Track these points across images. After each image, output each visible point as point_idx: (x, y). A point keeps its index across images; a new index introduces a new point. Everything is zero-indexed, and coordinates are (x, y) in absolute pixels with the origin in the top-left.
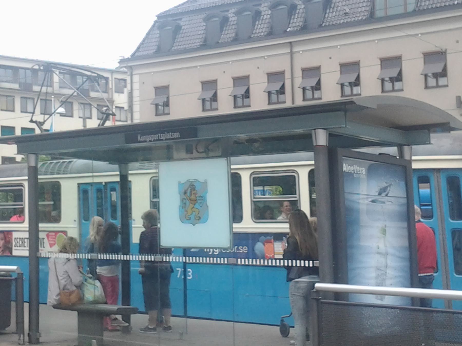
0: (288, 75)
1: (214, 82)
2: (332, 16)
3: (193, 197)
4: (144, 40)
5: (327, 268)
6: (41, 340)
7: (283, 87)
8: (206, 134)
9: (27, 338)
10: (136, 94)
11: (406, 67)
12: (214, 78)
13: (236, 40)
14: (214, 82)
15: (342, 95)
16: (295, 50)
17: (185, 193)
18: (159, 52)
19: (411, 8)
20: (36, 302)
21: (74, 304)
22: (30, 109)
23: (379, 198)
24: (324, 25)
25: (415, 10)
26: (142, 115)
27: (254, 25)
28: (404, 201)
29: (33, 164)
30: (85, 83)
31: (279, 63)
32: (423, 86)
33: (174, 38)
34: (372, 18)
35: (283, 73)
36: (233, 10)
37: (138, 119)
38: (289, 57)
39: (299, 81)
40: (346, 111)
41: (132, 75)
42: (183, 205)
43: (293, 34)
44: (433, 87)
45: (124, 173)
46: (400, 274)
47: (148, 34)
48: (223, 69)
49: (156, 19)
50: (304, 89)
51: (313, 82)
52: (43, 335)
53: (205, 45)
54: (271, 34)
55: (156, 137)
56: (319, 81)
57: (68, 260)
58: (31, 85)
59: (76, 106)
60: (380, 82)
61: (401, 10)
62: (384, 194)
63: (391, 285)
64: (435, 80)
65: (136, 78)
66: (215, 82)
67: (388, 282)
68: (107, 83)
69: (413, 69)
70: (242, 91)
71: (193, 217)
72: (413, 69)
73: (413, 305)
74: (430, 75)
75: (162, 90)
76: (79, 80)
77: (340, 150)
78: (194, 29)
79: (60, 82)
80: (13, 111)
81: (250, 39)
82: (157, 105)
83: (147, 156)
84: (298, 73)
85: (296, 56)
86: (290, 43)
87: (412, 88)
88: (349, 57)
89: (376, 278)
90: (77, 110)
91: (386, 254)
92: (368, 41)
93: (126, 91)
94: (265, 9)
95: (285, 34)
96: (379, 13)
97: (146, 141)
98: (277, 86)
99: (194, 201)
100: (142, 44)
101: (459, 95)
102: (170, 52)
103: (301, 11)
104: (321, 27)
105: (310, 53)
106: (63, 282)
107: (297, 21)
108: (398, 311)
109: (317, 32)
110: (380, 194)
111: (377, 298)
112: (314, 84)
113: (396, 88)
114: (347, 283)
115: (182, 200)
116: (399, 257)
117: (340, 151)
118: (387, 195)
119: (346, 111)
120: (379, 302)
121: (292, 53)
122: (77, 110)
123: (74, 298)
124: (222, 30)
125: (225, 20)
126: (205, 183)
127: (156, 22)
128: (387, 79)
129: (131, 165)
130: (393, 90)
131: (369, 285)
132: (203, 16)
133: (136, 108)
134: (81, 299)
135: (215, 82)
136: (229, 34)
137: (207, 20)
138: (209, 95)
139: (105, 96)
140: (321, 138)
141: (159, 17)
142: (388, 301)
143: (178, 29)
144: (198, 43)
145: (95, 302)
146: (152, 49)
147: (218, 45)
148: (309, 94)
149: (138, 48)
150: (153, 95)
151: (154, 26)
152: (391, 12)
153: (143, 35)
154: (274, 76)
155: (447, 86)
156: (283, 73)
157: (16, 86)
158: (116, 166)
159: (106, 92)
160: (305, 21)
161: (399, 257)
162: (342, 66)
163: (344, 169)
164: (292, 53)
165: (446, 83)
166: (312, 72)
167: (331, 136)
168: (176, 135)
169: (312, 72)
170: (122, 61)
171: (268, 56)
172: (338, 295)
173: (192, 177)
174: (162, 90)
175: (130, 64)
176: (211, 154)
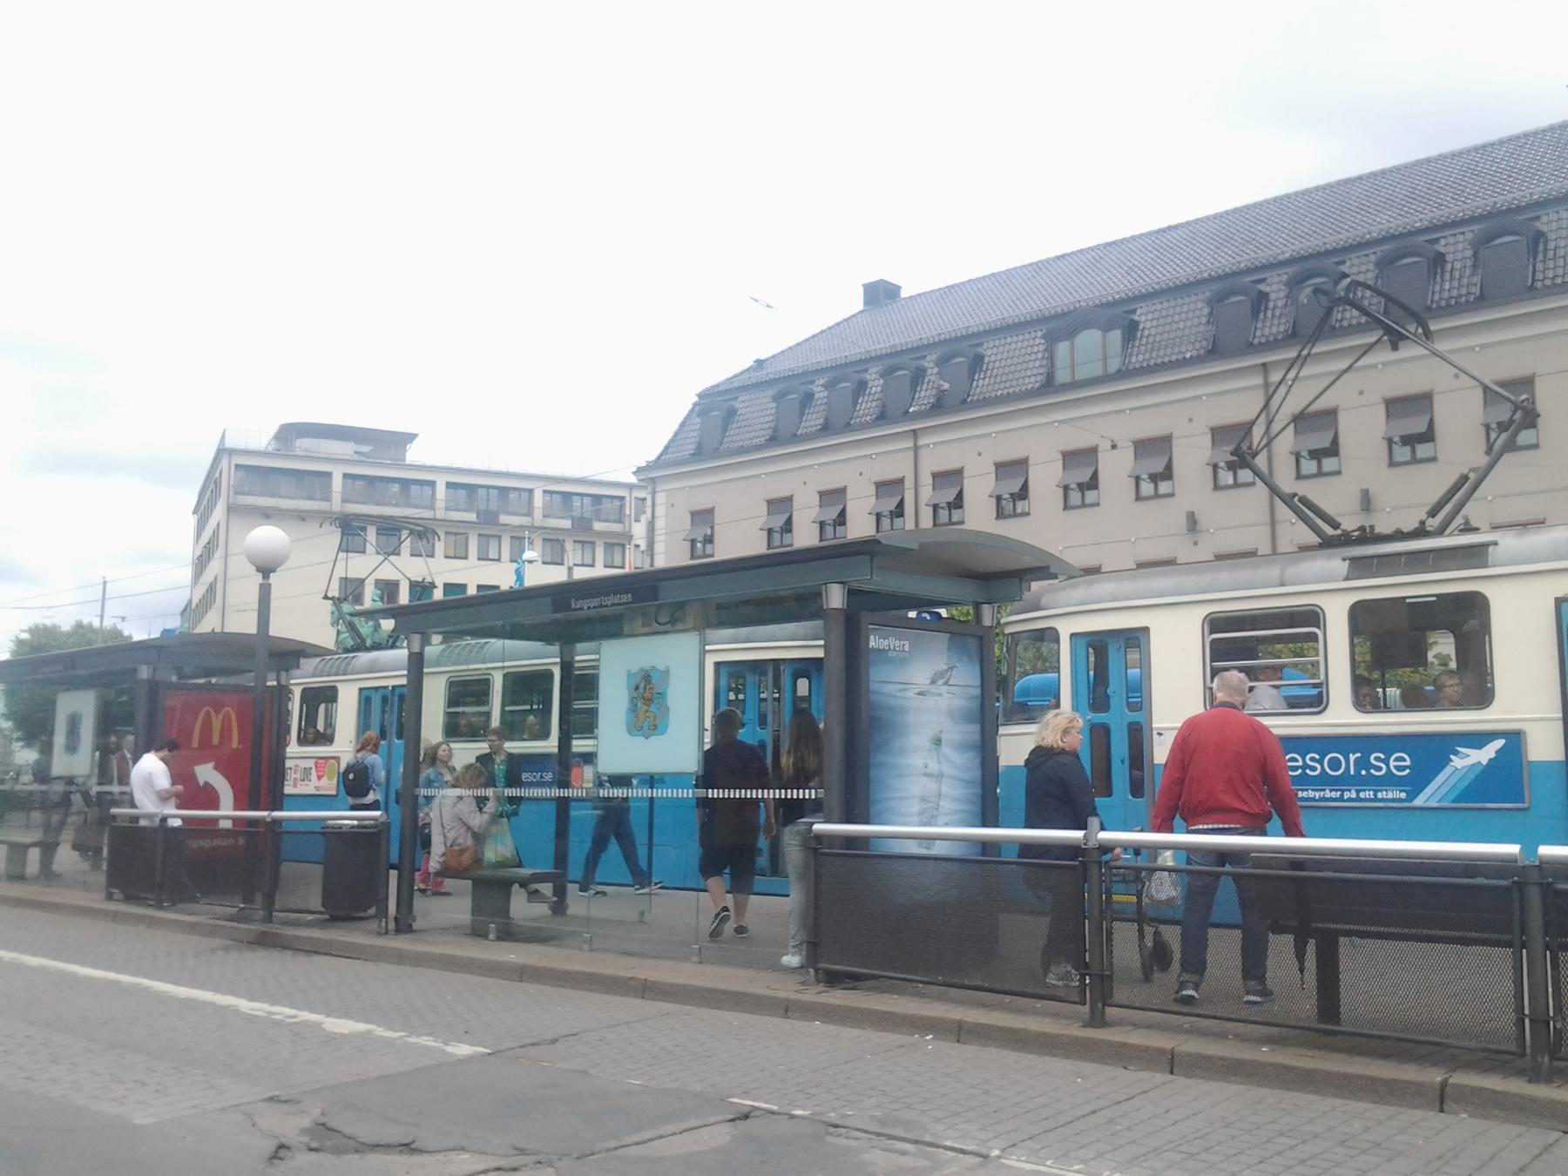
0: (909, 484)
1: (841, 492)
2: (983, 386)
3: (647, 695)
4: (676, 435)
5: (835, 803)
6: (415, 926)
7: (901, 505)
8: (670, 594)
9: (392, 925)
10: (660, 524)
11: (1443, 412)
12: (708, 506)
13: (826, 429)
14: (841, 492)
15: (769, 547)
16: (921, 443)
17: (637, 688)
18: (699, 454)
19: (1114, 365)
20: (408, 868)
21: (466, 869)
22: (493, 554)
23: (933, 688)
24: (1539, 284)
25: (1119, 371)
26: (669, 554)
27: (855, 403)
28: (978, 692)
29: (416, 649)
30: (585, 510)
31: (896, 466)
32: (1211, 485)
33: (725, 430)
34: (1049, 385)
35: (901, 481)
36: (822, 381)
37: (661, 562)
38: (911, 453)
39: (927, 493)
40: (872, 555)
41: (654, 493)
42: (633, 709)
43: (919, 416)
44: (1149, 498)
45: (567, 659)
46: (966, 807)
47: (683, 425)
48: (803, 479)
49: (696, 399)
50: (936, 507)
51: (950, 495)
52: (419, 919)
53: (774, 440)
54: (883, 417)
55: (596, 602)
56: (844, 510)
57: (460, 798)
58: (495, 515)
59: (569, 546)
60: (1133, 481)
61: (1096, 370)
62: (940, 682)
63: (946, 825)
64: (1314, 463)
65: (661, 498)
66: (790, 499)
67: (941, 820)
68: (622, 508)
69: (1046, 478)
70: (832, 513)
71: (645, 726)
72: (1046, 478)
73: (984, 854)
74: (1073, 486)
75: (702, 517)
76: (576, 503)
77: (866, 617)
78: (758, 413)
79: (544, 508)
80: (466, 558)
81: (848, 427)
82: (693, 542)
83: (610, 627)
84: (926, 479)
85: (923, 453)
86: (1264, 365)
87: (979, 516)
88: (1010, 452)
89: (921, 813)
90: (572, 554)
91: (939, 776)
92: (969, 438)
93: (643, 519)
94: (1275, 287)
95: (906, 416)
96: (1062, 376)
97: (585, 607)
98: (892, 504)
99: (648, 701)
100: (672, 441)
101: (1364, 486)
102: (717, 453)
103: (1280, 303)
104: (964, 404)
105: (941, 451)
106: (451, 835)
107: (925, 396)
108: (955, 867)
109: (1475, 310)
110: (933, 682)
111: (920, 846)
112: (951, 499)
113: (1088, 501)
114: (868, 823)
115: (633, 700)
116: (967, 782)
117: (866, 617)
118: (946, 683)
119: (872, 555)
120: (924, 852)
121: (916, 448)
122: (572, 554)
123: (466, 859)
124: (802, 414)
125: (809, 397)
126: (667, 672)
127: (695, 405)
128: (1073, 486)
129: (580, 646)
130: (951, 523)
131: (906, 824)
132: (771, 392)
133: (659, 547)
134: (478, 860)
135: (790, 499)
136: (813, 420)
137: (779, 397)
138: (778, 521)
139: (617, 527)
140: (836, 598)
141: (700, 396)
142: (939, 849)
143: (731, 414)
144: (765, 435)
145: (501, 864)
146: (690, 448)
147: (795, 438)
148: (943, 515)
149: (667, 448)
150: (688, 525)
151: (692, 411)
152: (1081, 374)
153: (675, 427)
154: (888, 487)
155: (1339, 473)
156: (901, 481)
157: (472, 517)
158: (556, 648)
159: (620, 521)
160: (827, 419)
161: (967, 782)
162: (822, 494)
163: (872, 644)
164: (916, 448)
165: (1336, 468)
166: (949, 478)
167: (852, 593)
168: (627, 598)
169: (949, 478)
170: (639, 471)
171: (1483, 346)
172: (851, 841)
173: (647, 665)
174: (702, 517)
175: (650, 474)
176: (680, 626)
